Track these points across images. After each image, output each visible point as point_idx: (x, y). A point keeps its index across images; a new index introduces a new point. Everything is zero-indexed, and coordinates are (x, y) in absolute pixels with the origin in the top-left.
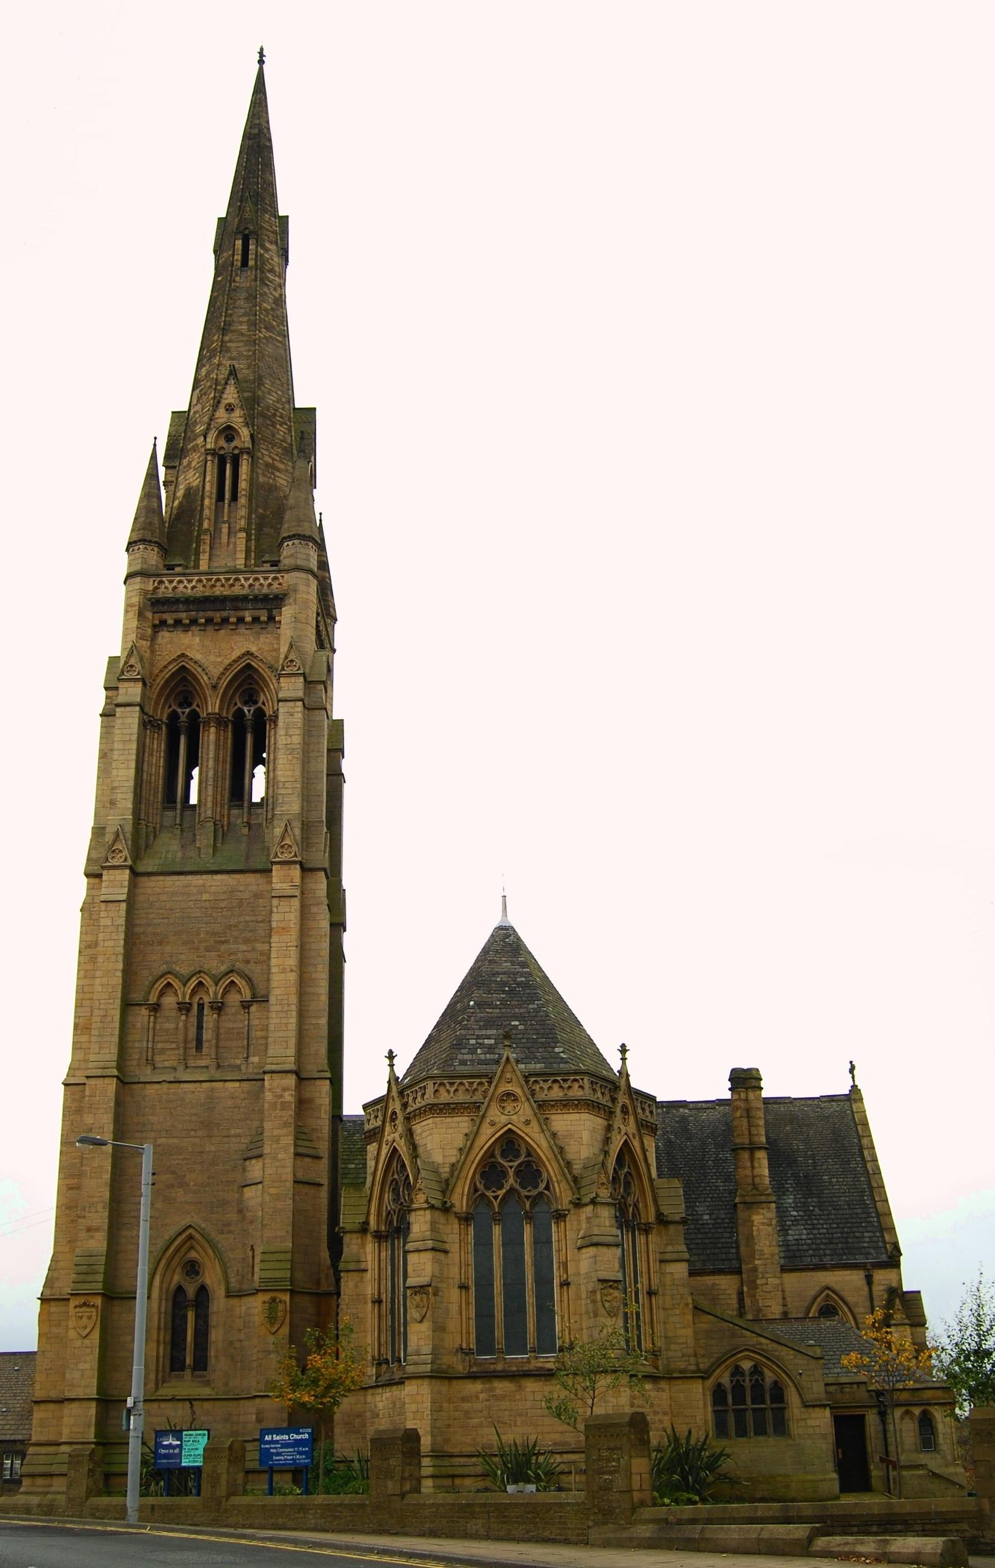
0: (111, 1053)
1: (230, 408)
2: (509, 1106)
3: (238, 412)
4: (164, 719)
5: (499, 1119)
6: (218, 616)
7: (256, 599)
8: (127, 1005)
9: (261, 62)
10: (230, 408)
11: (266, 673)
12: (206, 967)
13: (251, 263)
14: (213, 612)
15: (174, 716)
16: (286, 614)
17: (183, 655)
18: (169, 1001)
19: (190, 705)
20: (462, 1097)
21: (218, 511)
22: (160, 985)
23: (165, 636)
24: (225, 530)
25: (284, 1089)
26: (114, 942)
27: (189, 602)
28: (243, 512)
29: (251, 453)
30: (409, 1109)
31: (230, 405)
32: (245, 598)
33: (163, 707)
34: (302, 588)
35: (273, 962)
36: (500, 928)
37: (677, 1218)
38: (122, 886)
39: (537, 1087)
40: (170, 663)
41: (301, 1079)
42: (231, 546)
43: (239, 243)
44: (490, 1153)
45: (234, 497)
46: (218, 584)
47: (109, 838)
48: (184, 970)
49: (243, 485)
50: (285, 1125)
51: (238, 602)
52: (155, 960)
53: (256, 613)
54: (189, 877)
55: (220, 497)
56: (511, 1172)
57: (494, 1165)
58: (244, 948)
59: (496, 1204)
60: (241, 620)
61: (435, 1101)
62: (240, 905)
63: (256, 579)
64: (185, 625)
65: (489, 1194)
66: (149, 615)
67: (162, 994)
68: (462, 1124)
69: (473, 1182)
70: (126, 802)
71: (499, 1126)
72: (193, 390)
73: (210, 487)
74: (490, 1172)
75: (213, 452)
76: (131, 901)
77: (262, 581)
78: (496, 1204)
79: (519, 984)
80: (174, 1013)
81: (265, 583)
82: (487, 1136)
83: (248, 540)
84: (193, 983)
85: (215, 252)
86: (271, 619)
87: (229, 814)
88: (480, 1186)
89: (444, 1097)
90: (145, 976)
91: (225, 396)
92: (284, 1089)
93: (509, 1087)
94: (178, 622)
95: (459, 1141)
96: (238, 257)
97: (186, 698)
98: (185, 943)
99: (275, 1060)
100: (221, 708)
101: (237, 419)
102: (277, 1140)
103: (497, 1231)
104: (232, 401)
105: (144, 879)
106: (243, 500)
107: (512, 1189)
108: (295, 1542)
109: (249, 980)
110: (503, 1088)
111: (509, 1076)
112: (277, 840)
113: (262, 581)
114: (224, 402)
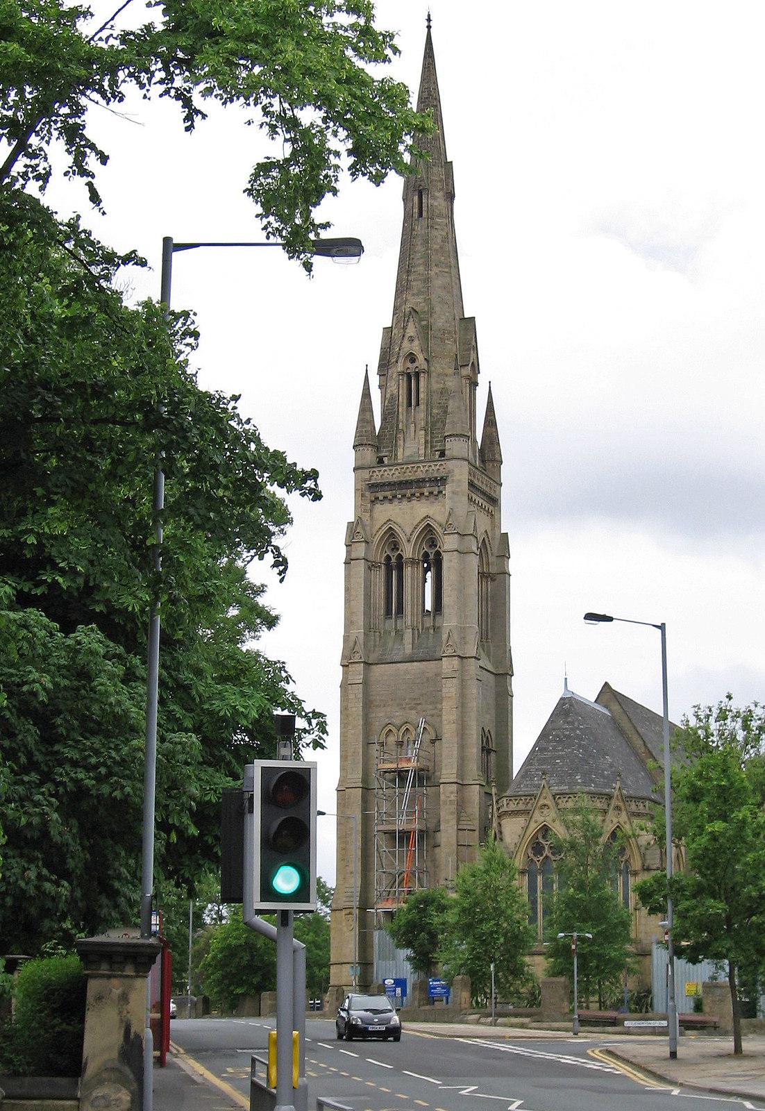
0: (358, 775)
1: (411, 339)
2: (545, 811)
3: (416, 342)
4: (383, 562)
5: (539, 818)
6: (408, 493)
7: (430, 480)
8: (367, 744)
9: (429, 27)
10: (411, 339)
11: (439, 530)
12: (409, 720)
13: (424, 214)
14: (406, 489)
15: (388, 558)
16: (448, 490)
17: (389, 520)
18: (392, 739)
19: (398, 549)
20: (521, 807)
21: (408, 412)
22: (385, 731)
23: (378, 507)
24: (412, 429)
25: (452, 793)
26: (357, 708)
27: (391, 485)
28: (422, 415)
29: (428, 372)
30: (501, 810)
31: (411, 337)
32: (423, 480)
33: (381, 553)
34: (457, 471)
35: (444, 717)
36: (563, 701)
37: (654, 867)
38: (360, 674)
39: (560, 801)
40: (382, 526)
41: (462, 786)
42: (417, 440)
43: (416, 198)
44: (535, 837)
45: (418, 404)
46: (408, 471)
47: (352, 644)
48: (397, 722)
49: (422, 396)
50: (452, 813)
51: (420, 482)
52: (380, 716)
53: (431, 489)
54: (398, 665)
55: (409, 404)
56: (546, 847)
57: (538, 843)
58: (431, 707)
59: (538, 864)
60: (422, 494)
61: (507, 810)
62: (428, 680)
63: (430, 466)
64: (390, 500)
65: (536, 859)
66: (367, 494)
67: (387, 735)
68: (521, 821)
69: (526, 853)
70: (360, 619)
71: (539, 822)
72: (394, 315)
73: (403, 399)
74: (537, 848)
75: (401, 373)
76: (366, 683)
77: (433, 468)
78: (538, 864)
79: (565, 736)
80: (394, 747)
81: (435, 470)
82: (534, 827)
83: (426, 435)
84: (403, 729)
85: (404, 200)
86: (440, 492)
87: (422, 621)
88: (531, 855)
89: (512, 807)
90: (377, 726)
91: (407, 331)
92: (452, 793)
93: (546, 802)
94: (385, 498)
95: (520, 831)
96: (416, 210)
97: (395, 545)
98: (398, 705)
99: (447, 776)
100: (414, 553)
101: (416, 347)
102: (448, 821)
103: (539, 878)
104: (412, 334)
105: (373, 667)
106: (422, 407)
107: (547, 857)
108: (514, 1040)
109: (433, 727)
110: (542, 802)
111: (544, 795)
112: (444, 642)
113: (433, 468)
114: (407, 335)
